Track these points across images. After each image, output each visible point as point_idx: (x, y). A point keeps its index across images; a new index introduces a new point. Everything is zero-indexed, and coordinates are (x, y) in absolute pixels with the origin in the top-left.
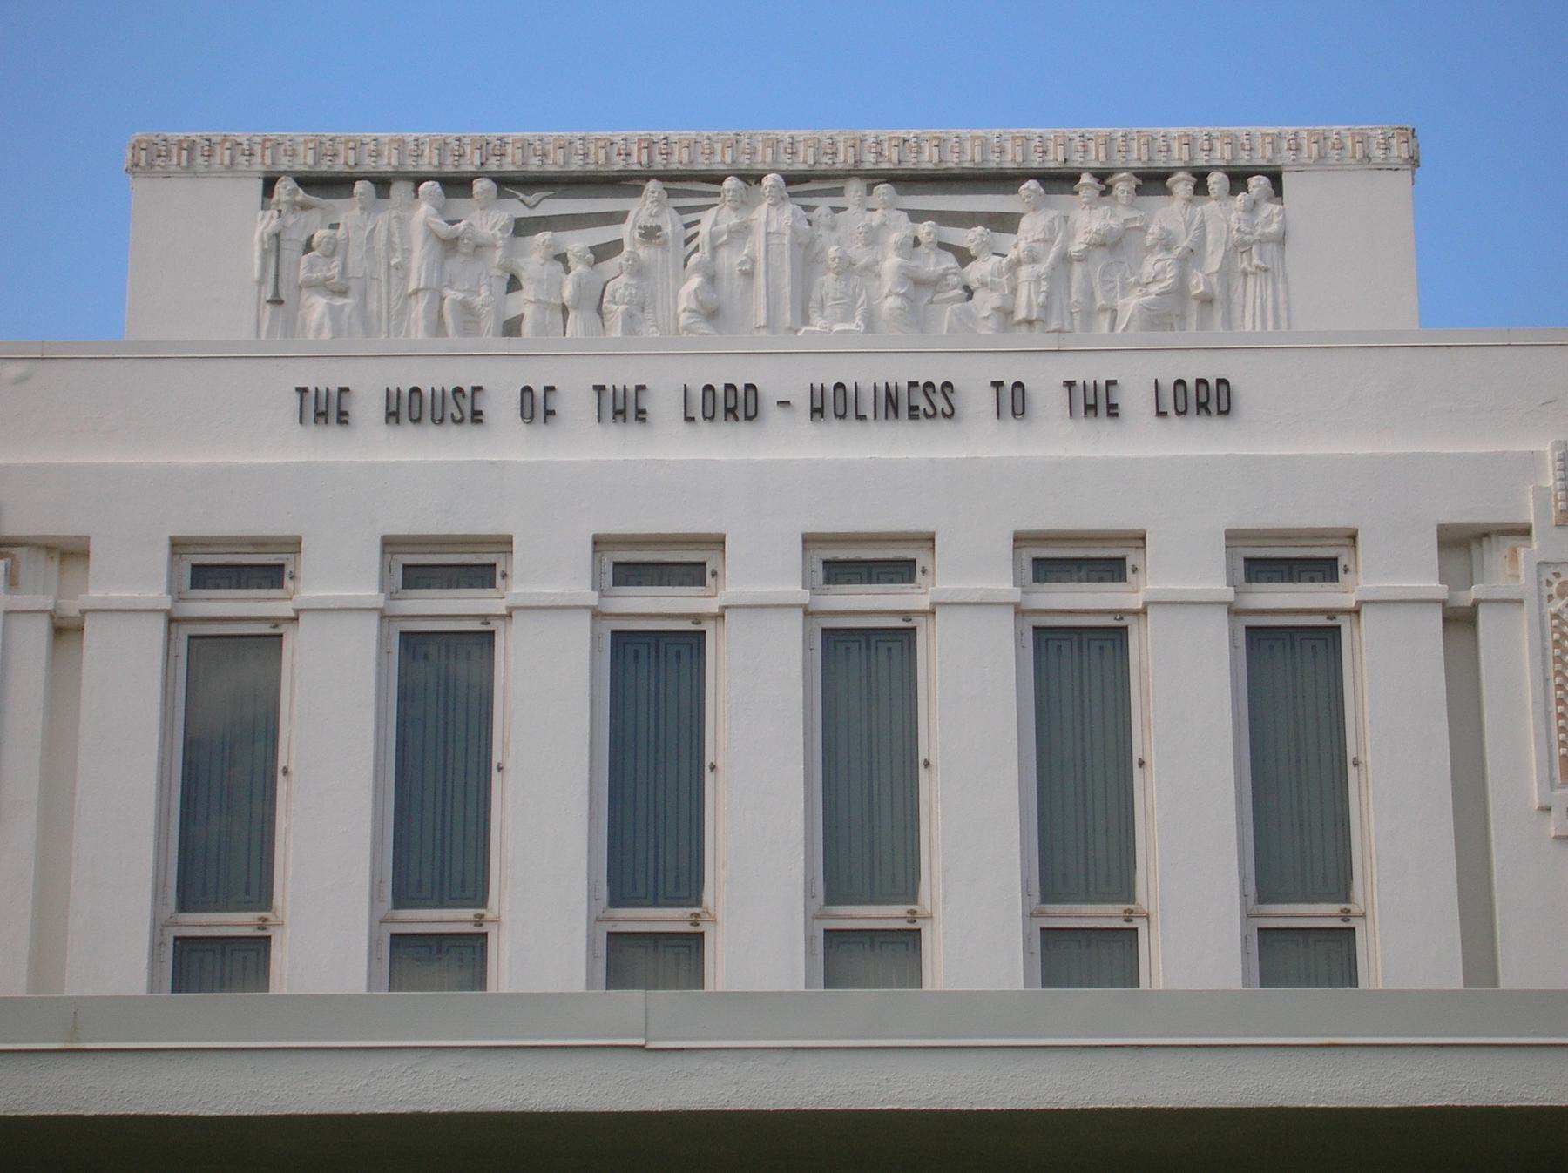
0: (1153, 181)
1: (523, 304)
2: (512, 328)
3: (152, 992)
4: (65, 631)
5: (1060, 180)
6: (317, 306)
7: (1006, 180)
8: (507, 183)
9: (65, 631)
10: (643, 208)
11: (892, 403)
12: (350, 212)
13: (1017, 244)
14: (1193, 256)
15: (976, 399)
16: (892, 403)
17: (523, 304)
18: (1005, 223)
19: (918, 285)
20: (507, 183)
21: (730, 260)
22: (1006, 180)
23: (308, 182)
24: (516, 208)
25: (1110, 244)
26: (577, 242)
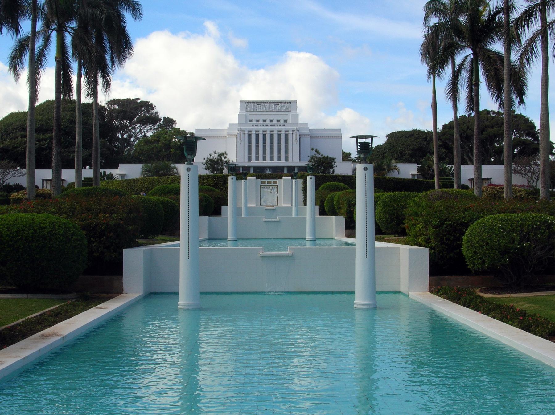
0: (285, 103)
1: (257, 108)
2: (257, 110)
3: (298, 216)
4: (244, 134)
5: (281, 103)
6: (248, 109)
7: (279, 103)
8: (256, 103)
9: (244, 134)
10: (262, 104)
11: (273, 125)
12: (249, 104)
13: (279, 106)
14: (287, 107)
15: (276, 125)
16: (273, 125)
17: (257, 108)
18: (279, 105)
19: (275, 108)
20: (256, 103)
21: (267, 106)
22: (279, 103)
23: (248, 103)
24: (257, 104)
25: (283, 106)
26: (260, 106)
